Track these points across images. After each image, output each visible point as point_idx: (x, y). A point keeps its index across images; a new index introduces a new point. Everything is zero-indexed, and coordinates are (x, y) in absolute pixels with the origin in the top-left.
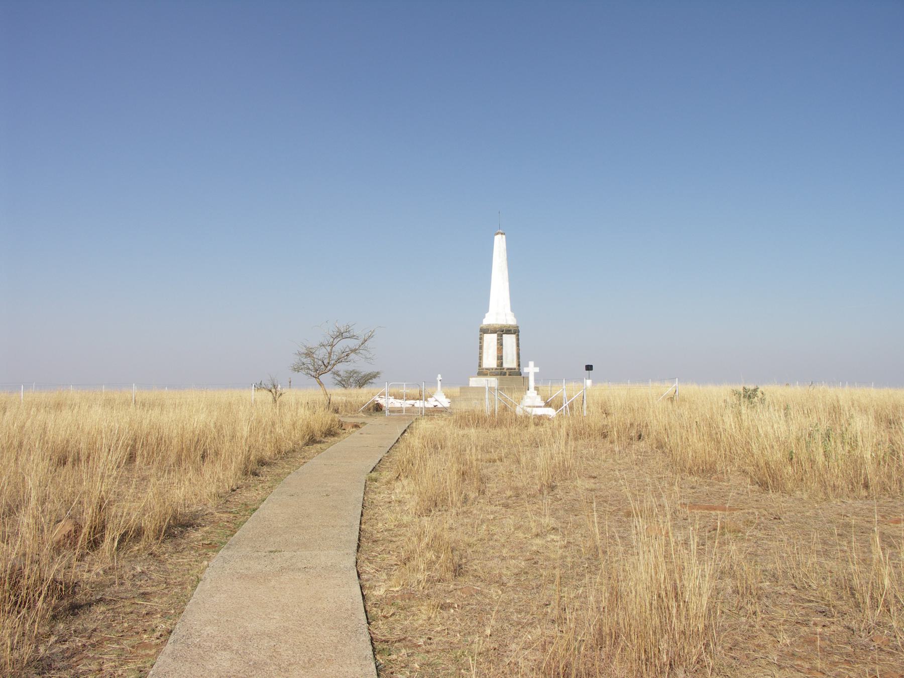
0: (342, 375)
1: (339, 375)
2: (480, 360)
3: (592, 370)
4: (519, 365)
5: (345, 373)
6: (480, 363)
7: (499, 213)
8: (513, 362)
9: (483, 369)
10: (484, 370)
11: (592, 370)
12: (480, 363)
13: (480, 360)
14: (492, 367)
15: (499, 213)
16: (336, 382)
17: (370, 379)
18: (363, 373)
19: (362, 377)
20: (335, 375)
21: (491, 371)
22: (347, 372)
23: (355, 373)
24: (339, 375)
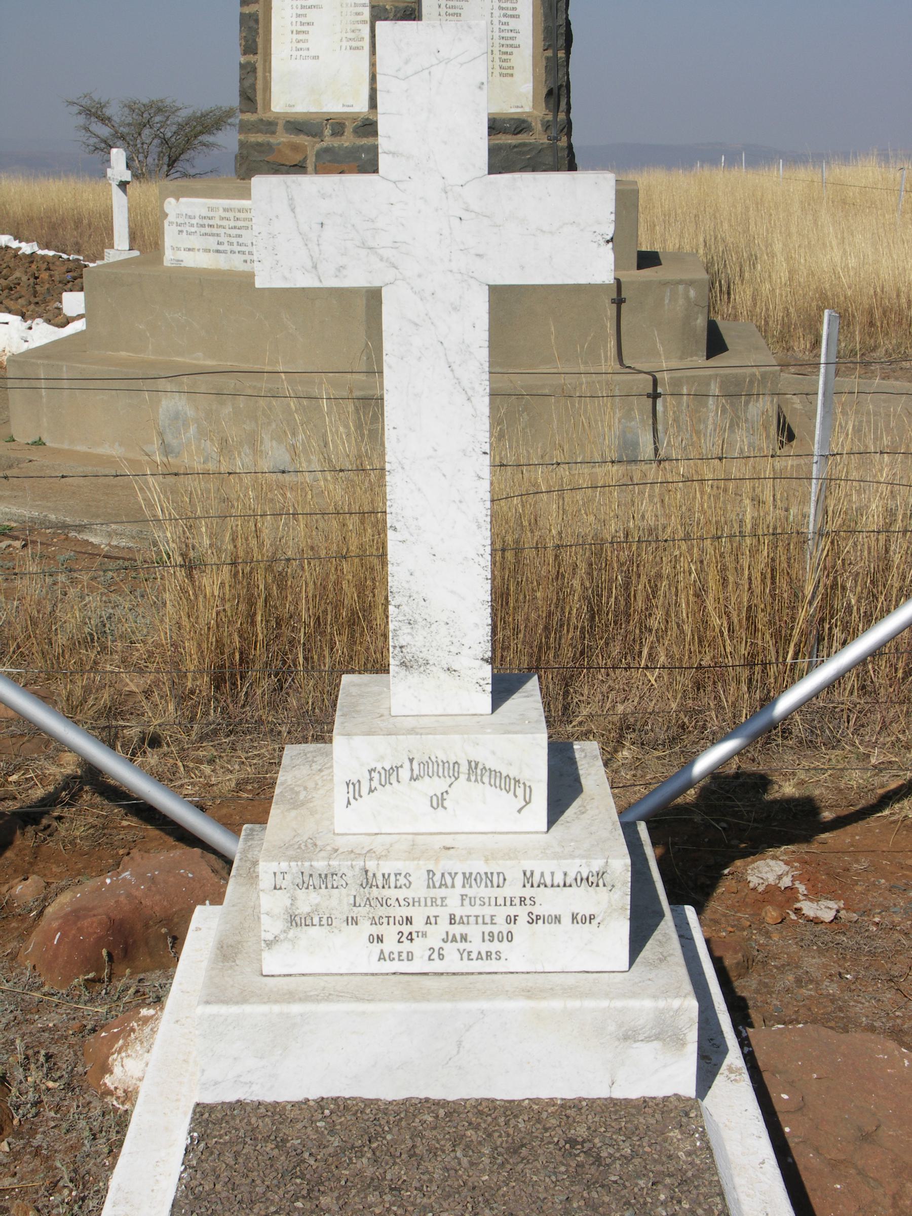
0: (116, 119)
1: (104, 120)
2: (250, 48)
3: (221, 904)
4: (373, 103)
5: (126, 110)
6: (248, 70)
7: (444, 475)
8: (507, 72)
9: (269, 126)
10: (282, 138)
11: (221, 904)
12: (248, 70)
13: (250, 48)
14: (333, 106)
15: (444, 475)
16: (93, 140)
17: (202, 133)
18: (184, 114)
19: (181, 127)
20: (93, 119)
21: (329, 141)
22: (130, 107)
23: (159, 110)
24: (104, 120)
